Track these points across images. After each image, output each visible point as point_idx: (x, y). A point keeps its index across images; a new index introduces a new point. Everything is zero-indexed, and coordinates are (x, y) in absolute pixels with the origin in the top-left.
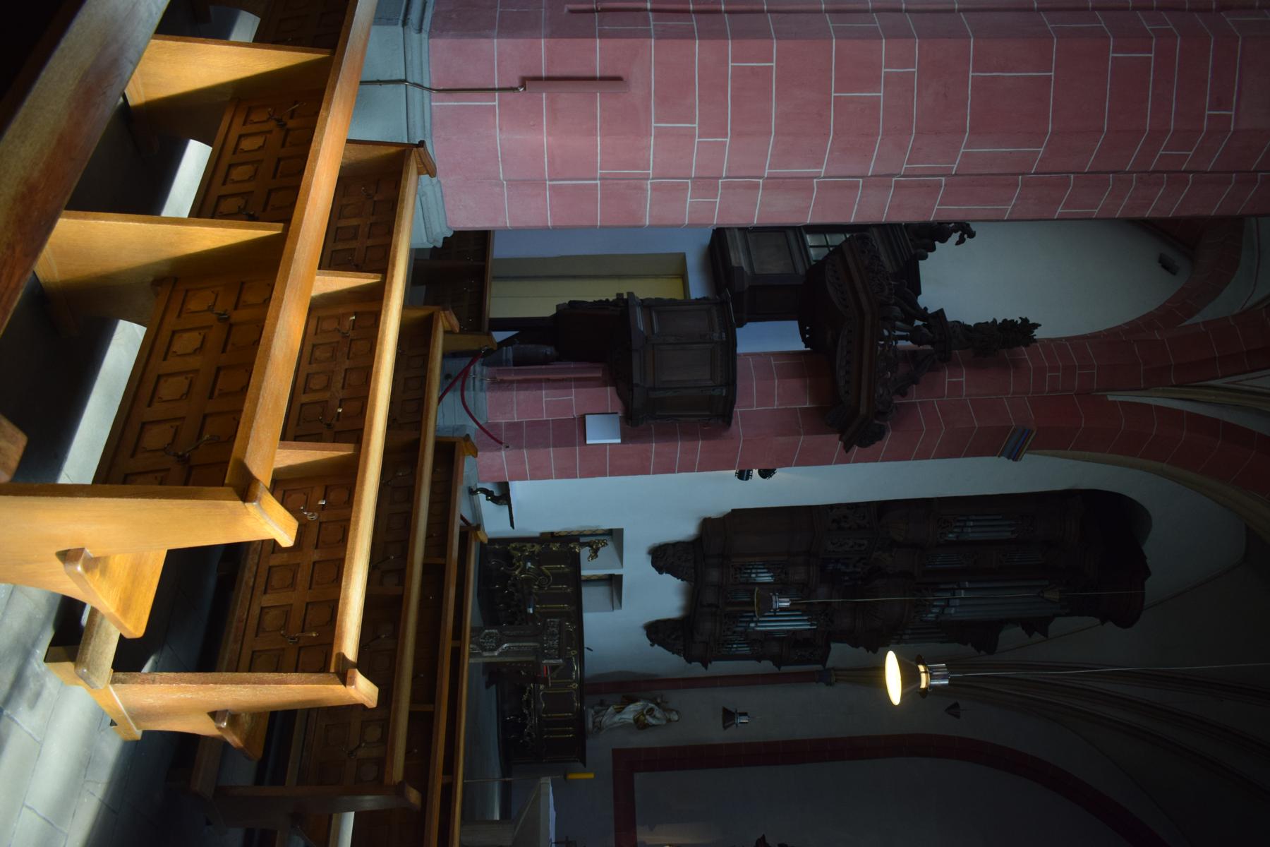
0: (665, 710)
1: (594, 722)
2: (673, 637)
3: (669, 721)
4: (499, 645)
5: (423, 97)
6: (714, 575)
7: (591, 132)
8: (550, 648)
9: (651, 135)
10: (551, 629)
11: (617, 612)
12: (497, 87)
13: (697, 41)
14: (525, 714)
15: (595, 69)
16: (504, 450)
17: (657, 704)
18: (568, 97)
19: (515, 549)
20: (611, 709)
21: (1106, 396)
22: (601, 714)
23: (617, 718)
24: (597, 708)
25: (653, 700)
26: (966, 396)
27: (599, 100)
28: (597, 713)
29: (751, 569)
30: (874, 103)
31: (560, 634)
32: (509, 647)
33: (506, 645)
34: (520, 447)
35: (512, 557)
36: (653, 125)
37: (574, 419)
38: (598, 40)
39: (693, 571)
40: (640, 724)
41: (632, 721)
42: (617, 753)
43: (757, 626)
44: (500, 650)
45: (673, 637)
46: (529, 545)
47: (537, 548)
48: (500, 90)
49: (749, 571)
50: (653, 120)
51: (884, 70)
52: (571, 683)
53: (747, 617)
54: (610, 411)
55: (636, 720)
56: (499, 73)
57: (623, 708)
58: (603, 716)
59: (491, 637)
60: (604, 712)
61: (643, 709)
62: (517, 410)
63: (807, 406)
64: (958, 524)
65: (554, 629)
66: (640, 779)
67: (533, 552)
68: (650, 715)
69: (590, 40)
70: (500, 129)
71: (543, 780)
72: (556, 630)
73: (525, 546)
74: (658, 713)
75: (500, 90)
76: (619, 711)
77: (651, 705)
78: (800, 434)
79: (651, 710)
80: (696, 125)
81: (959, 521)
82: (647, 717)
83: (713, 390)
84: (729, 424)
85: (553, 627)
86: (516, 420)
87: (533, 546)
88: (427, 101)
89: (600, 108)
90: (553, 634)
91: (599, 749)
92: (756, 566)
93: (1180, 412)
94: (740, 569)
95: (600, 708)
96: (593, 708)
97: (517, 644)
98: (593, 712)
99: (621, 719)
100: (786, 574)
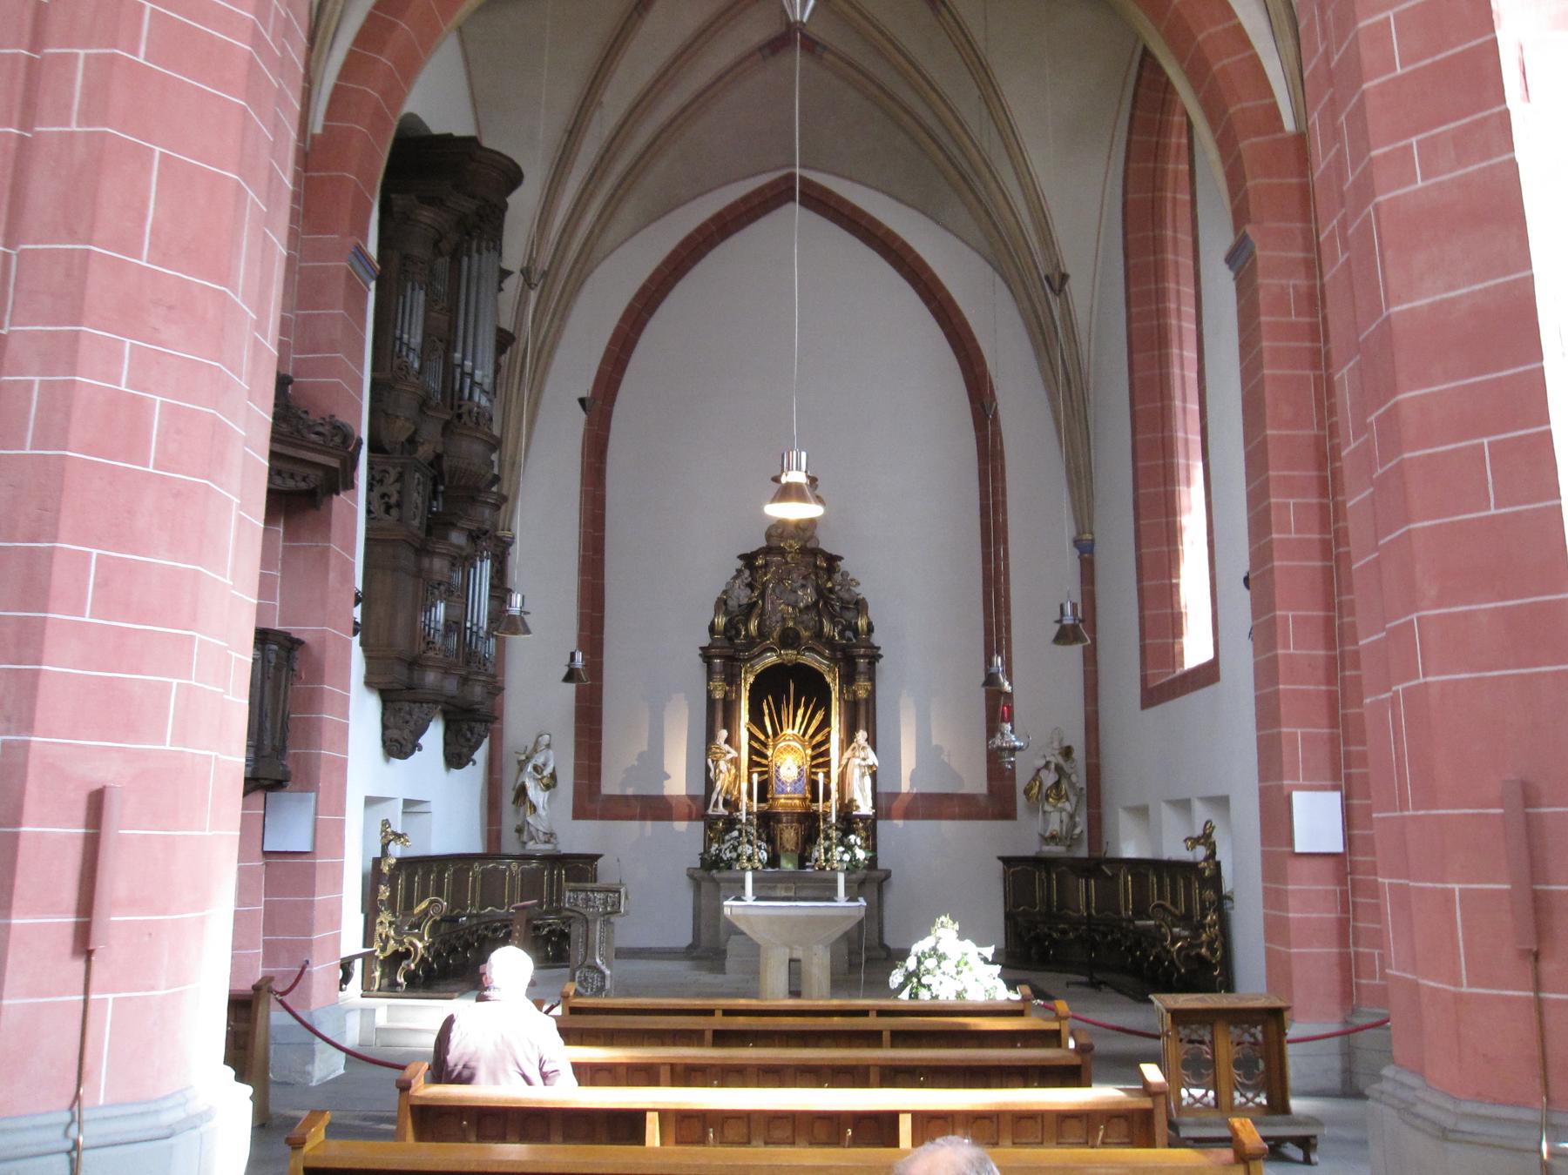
0: (535, 750)
1: (546, 842)
2: (469, 735)
3: (548, 746)
4: (595, 968)
5: (95, 1119)
6: (431, 678)
7: (1286, 891)
8: (605, 903)
9: (182, 752)
10: (580, 902)
11: (433, 807)
12: (81, 997)
13: (44, 667)
14: (549, 932)
15: (71, 837)
16: (312, 967)
17: (528, 759)
18: (115, 880)
19: (383, 949)
20: (530, 819)
21: (313, 136)
22: (534, 833)
23: (541, 811)
24: (525, 837)
25: (522, 765)
26: (292, 313)
27: (121, 829)
28: (532, 838)
29: (430, 629)
30: (171, 412)
31: (586, 891)
32: (601, 955)
33: (598, 961)
34: (309, 943)
35: (396, 952)
36: (167, 747)
37: (266, 864)
38: (23, 829)
39: (424, 705)
40: (551, 784)
41: (547, 793)
42: (580, 813)
43: (482, 628)
44: (603, 968)
45: (469, 735)
46: (379, 929)
47: (385, 917)
48: (86, 991)
49: (432, 631)
50: (162, 747)
51: (123, 388)
52: (511, 872)
53: (471, 636)
54: (262, 812)
55: (547, 787)
56: (60, 994)
57: (530, 802)
58: (538, 830)
59: (586, 979)
60: (532, 829)
61: (535, 779)
62: (247, 949)
63: (282, 530)
64: (404, 353)
65: (580, 897)
66: (611, 784)
67: (391, 923)
68: (542, 770)
69: (22, 844)
70: (153, 988)
71: (727, 911)
72: (582, 895)
73: (381, 935)
74: (539, 759)
75: (86, 991)
76: (534, 808)
77: (530, 768)
78: (328, 548)
79: (535, 768)
80: (175, 682)
81: (400, 351)
82: (545, 773)
83: (269, 662)
84: (300, 643)
85: (576, 899)
86: (261, 950)
87: (381, 923)
88: (99, 1114)
89: (133, 829)
90: (587, 900)
91: (577, 837)
92: (427, 622)
93: (351, 54)
94: (428, 643)
95: (526, 833)
96: (525, 843)
97: (597, 947)
98: (531, 843)
99: (543, 807)
100: (439, 584)
